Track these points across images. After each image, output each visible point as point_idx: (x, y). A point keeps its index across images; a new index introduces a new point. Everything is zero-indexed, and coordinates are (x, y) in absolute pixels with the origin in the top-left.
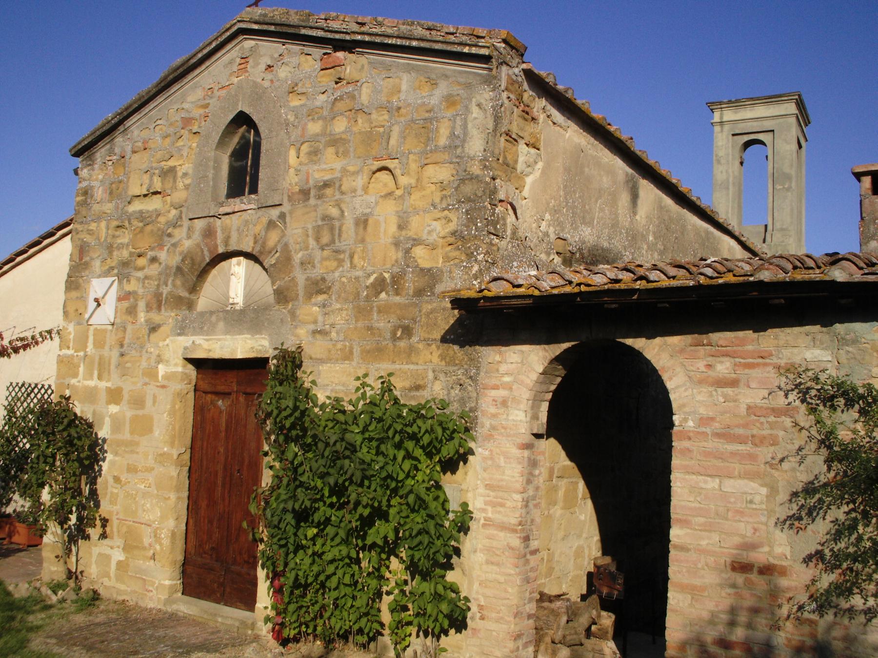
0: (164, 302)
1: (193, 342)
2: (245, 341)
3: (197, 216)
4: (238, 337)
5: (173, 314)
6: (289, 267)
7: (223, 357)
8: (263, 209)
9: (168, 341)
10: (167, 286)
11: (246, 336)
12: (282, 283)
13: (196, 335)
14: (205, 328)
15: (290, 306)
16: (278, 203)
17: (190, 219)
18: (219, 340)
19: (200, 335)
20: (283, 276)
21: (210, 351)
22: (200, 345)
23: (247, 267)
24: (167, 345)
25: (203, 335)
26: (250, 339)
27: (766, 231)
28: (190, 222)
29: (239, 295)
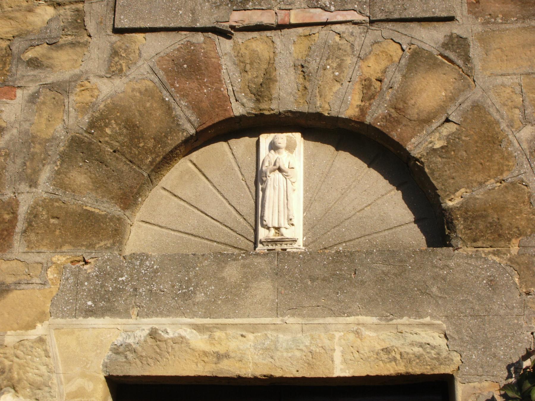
0: (20, 226)
1: (153, 334)
2: (357, 333)
3: (142, 25)
4: (330, 320)
5: (60, 259)
6: (497, 157)
7: (278, 373)
8: (390, 25)
9: (40, 330)
10: (33, 184)
11: (362, 319)
12: (479, 194)
13: (161, 314)
14: (200, 297)
15: (515, 249)
16: (444, 14)
17: (117, 31)
18: (254, 328)
19: (184, 314)
20: (480, 178)
21: (219, 357)
22: (181, 340)
23: (309, 159)
24: (41, 340)
25: (194, 315)
26: (376, 328)
27: (211, 240)
28: (115, 38)
29: (294, 221)
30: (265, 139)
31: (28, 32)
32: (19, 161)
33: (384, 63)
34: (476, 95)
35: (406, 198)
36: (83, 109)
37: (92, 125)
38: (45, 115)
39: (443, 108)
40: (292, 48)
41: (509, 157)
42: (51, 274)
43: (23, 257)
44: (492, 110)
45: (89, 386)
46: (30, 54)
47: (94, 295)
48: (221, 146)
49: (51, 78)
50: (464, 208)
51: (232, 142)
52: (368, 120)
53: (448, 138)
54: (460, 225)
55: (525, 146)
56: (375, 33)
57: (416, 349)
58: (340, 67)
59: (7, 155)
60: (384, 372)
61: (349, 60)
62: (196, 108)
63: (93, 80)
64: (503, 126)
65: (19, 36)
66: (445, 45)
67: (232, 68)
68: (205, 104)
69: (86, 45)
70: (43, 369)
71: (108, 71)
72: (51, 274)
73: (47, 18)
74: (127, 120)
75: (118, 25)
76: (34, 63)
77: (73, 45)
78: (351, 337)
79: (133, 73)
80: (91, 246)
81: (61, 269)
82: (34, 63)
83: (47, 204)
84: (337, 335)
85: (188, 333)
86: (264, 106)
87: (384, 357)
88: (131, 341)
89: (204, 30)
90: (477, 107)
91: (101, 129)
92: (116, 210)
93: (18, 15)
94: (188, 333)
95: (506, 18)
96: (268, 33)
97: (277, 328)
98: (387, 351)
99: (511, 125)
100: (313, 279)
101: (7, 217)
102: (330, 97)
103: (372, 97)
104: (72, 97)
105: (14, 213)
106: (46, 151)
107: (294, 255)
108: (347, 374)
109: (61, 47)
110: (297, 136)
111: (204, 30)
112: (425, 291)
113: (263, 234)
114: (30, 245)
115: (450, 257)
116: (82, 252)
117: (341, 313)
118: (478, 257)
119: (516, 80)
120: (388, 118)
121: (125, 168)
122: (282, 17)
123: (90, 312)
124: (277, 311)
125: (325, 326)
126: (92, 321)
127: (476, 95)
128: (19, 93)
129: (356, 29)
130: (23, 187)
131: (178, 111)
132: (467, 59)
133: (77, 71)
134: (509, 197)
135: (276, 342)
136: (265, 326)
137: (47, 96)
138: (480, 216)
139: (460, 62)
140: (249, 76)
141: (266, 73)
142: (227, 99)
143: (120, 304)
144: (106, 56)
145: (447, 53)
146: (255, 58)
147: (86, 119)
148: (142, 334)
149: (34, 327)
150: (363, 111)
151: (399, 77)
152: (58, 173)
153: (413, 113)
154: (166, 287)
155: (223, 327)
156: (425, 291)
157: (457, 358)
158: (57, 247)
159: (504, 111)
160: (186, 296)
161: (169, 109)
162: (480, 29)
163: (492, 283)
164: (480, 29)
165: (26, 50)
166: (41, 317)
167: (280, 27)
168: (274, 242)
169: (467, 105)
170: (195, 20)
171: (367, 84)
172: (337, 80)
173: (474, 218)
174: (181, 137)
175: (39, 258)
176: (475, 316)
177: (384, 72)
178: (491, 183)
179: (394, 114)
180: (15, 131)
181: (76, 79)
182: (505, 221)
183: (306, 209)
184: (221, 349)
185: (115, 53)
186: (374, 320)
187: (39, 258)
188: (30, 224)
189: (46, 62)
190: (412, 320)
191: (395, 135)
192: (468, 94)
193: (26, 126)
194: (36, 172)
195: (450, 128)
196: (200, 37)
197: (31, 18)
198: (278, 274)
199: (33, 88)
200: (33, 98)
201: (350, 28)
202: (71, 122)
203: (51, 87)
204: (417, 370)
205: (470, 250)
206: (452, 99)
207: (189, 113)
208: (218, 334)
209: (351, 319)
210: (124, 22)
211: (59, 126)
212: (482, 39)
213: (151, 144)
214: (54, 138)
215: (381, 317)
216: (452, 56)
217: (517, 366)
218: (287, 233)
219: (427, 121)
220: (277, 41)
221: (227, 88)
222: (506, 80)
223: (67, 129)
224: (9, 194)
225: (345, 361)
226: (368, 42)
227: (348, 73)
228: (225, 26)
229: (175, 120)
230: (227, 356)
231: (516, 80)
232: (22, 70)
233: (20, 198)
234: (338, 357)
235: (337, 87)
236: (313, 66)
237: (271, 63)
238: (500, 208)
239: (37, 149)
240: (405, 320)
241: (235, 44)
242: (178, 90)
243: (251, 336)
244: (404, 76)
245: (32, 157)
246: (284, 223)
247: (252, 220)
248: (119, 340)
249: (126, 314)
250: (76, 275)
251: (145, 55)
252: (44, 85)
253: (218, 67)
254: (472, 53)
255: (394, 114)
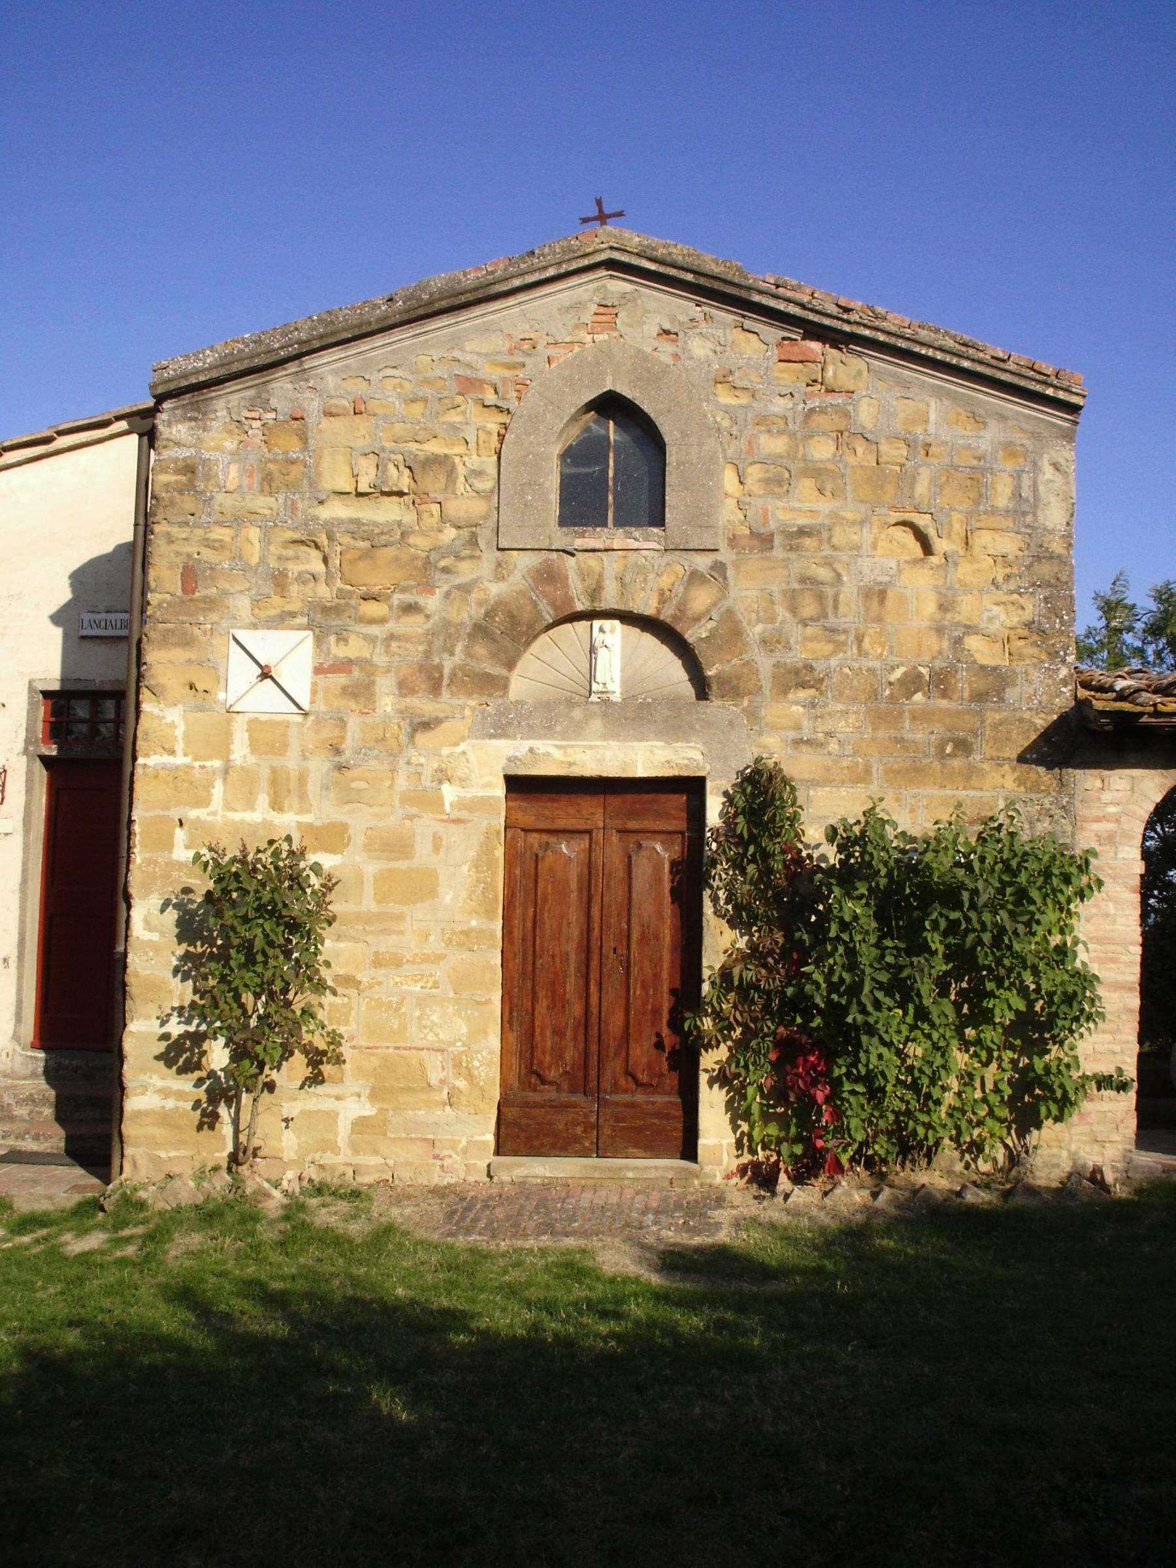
0: (446, 681)
1: (531, 750)
2: (652, 751)
4: (635, 744)
5: (472, 703)
6: (739, 644)
7: (605, 775)
9: (462, 747)
10: (452, 654)
12: (727, 668)
13: (535, 738)
14: (559, 728)
15: (746, 703)
17: (499, 549)
18: (591, 748)
20: (728, 657)
21: (570, 764)
22: (547, 754)
24: (464, 753)
25: (555, 739)
26: (663, 748)
28: (499, 554)
30: (597, 624)
31: (440, 547)
32: (441, 638)
33: (673, 578)
34: (728, 603)
35: (684, 665)
36: (480, 603)
37: (487, 614)
38: (456, 607)
39: (708, 611)
40: (614, 565)
41: (746, 644)
42: (467, 712)
43: (449, 701)
44: (739, 614)
45: (494, 781)
46: (442, 563)
47: (495, 725)
48: (568, 626)
49: (457, 581)
50: (717, 676)
51: (575, 624)
52: (662, 618)
53: (710, 631)
54: (714, 687)
55: (757, 637)
56: (669, 557)
57: (686, 762)
58: (645, 580)
59: (433, 634)
60: (667, 774)
61: (651, 576)
62: (553, 604)
63: (486, 584)
64: (744, 624)
65: (434, 549)
66: (712, 568)
67: (575, 577)
68: (559, 602)
69: (479, 558)
70: (466, 770)
71: (495, 577)
72: (467, 712)
73: (452, 537)
74: (509, 611)
75: (501, 546)
76: (446, 570)
77: (471, 557)
78: (648, 753)
79: (511, 579)
80: (490, 695)
81: (473, 709)
82: (446, 570)
83: (462, 668)
84: (640, 752)
85: (552, 751)
86: (596, 604)
87: (667, 765)
88: (517, 754)
89: (557, 550)
90: (730, 612)
91: (493, 618)
92: (503, 672)
93: (432, 534)
94: (552, 751)
95: (752, 549)
96: (599, 554)
97: (604, 748)
98: (668, 762)
99: (749, 624)
100: (626, 719)
101: (437, 675)
102: (638, 601)
103: (665, 602)
104: (473, 596)
105: (441, 673)
106: (458, 632)
107: (615, 704)
108: (645, 775)
109: (463, 559)
110: (617, 623)
111: (557, 550)
112: (692, 728)
113: (595, 687)
114: (453, 694)
115: (707, 707)
116: (484, 699)
117: (642, 740)
118: (724, 708)
119: (755, 593)
120: (675, 617)
121: (509, 645)
122: (607, 545)
123: (492, 736)
124: (604, 737)
125: (633, 747)
126: (494, 741)
127: (728, 603)
128: (437, 590)
129: (656, 554)
130: (446, 656)
131: (541, 607)
132: (725, 578)
133: (474, 576)
134: (745, 670)
135: (603, 756)
136: (597, 746)
137: (455, 594)
138: (554, 992)
139: (721, 580)
140: (587, 584)
141: (598, 582)
142: (572, 599)
143: (510, 731)
144: (493, 566)
145: (713, 573)
146: (590, 572)
147: (483, 611)
148: (525, 750)
149: (458, 745)
150: (659, 611)
151: (681, 589)
152: (467, 647)
153: (690, 613)
154: (537, 722)
155: (572, 746)
156: (692, 728)
157: (708, 767)
158: (470, 695)
159: (746, 614)
160: (550, 728)
161: (535, 605)
162: (734, 557)
163: (731, 723)
164: (734, 557)
165: (440, 560)
166: (463, 739)
167: (606, 550)
168: (602, 692)
169: (723, 609)
170: (551, 544)
171: (662, 593)
172: (643, 589)
173: (723, 683)
174: (545, 624)
175: (460, 702)
176: (719, 743)
177: (673, 585)
178: (735, 662)
179: (678, 614)
180: (436, 617)
181: (474, 582)
182: (742, 685)
183: (622, 670)
184: (571, 760)
185: (499, 565)
186: (661, 744)
187: (460, 702)
188: (452, 680)
189: (454, 569)
190: (684, 744)
191: (678, 628)
192: (724, 602)
193: (444, 614)
194: (453, 646)
195: (711, 624)
196: (554, 555)
197: (441, 536)
198: (605, 715)
199: (446, 588)
200: (447, 595)
201: (652, 553)
202: (473, 612)
203: (460, 587)
204: (685, 773)
205: (719, 703)
206: (714, 605)
207: (549, 608)
208: (569, 751)
209: (649, 743)
210: (504, 544)
211: (465, 615)
212: (736, 564)
213: (524, 629)
214: (462, 623)
215: (666, 742)
216: (716, 575)
217: (742, 772)
218: (610, 687)
219: (697, 619)
220: (605, 559)
221: (573, 592)
222: (749, 593)
223: (470, 617)
224: (437, 660)
225: (644, 768)
226: (663, 564)
227: (650, 584)
228: (569, 548)
229: (539, 612)
230: (574, 764)
231: (755, 593)
232: (438, 575)
233: (445, 663)
234: (639, 765)
235: (642, 594)
236: (628, 579)
237: (601, 575)
238: (739, 678)
239: (453, 630)
240: (679, 744)
241: (577, 562)
242: (541, 592)
243: (588, 752)
244: (685, 589)
245: (450, 636)
246: (608, 681)
247: (588, 676)
248: (510, 754)
249: (514, 738)
250: (482, 713)
251: (518, 567)
252: (453, 587)
253: (567, 577)
254: (728, 574)
255: (678, 614)
